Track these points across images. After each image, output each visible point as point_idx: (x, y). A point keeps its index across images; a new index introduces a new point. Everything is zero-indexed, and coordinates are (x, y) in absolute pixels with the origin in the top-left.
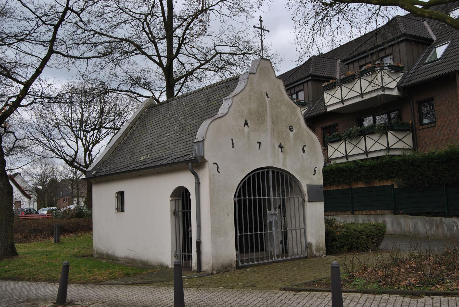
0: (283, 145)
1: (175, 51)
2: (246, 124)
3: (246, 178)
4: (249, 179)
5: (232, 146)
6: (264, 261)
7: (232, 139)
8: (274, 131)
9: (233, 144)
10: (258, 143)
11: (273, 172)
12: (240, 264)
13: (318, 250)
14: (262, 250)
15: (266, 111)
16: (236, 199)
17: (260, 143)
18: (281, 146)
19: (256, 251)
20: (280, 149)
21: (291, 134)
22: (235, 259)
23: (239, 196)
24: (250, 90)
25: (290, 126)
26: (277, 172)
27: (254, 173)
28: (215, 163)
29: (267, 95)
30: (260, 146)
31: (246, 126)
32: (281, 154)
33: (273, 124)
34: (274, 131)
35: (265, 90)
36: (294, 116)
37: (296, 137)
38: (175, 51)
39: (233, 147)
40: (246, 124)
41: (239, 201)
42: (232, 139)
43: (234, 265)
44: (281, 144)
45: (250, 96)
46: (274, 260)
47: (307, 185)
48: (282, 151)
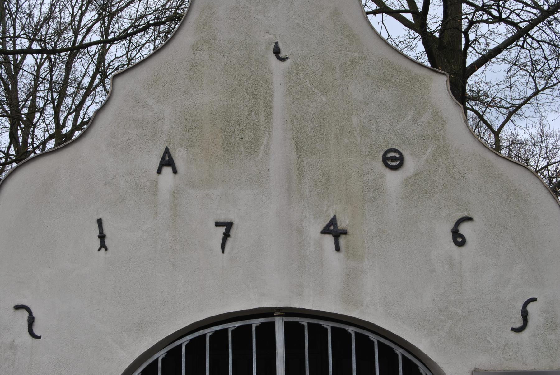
0: (342, 224)
1: (61, 122)
2: (167, 161)
3: (160, 355)
5: (98, 243)
7: (100, 222)
8: (300, 176)
9: (102, 237)
10: (218, 224)
11: (293, 332)
15: (268, 107)
17: (229, 226)
18: (333, 230)
20: (329, 240)
21: (393, 180)
24: (195, 47)
25: (385, 160)
26: (363, 341)
27: (201, 333)
29: (277, 52)
30: (227, 235)
31: (167, 171)
33: (297, 149)
34: (300, 176)
38: (61, 122)
39: (103, 246)
40: (167, 161)
42: (100, 222)
48: (338, 249)
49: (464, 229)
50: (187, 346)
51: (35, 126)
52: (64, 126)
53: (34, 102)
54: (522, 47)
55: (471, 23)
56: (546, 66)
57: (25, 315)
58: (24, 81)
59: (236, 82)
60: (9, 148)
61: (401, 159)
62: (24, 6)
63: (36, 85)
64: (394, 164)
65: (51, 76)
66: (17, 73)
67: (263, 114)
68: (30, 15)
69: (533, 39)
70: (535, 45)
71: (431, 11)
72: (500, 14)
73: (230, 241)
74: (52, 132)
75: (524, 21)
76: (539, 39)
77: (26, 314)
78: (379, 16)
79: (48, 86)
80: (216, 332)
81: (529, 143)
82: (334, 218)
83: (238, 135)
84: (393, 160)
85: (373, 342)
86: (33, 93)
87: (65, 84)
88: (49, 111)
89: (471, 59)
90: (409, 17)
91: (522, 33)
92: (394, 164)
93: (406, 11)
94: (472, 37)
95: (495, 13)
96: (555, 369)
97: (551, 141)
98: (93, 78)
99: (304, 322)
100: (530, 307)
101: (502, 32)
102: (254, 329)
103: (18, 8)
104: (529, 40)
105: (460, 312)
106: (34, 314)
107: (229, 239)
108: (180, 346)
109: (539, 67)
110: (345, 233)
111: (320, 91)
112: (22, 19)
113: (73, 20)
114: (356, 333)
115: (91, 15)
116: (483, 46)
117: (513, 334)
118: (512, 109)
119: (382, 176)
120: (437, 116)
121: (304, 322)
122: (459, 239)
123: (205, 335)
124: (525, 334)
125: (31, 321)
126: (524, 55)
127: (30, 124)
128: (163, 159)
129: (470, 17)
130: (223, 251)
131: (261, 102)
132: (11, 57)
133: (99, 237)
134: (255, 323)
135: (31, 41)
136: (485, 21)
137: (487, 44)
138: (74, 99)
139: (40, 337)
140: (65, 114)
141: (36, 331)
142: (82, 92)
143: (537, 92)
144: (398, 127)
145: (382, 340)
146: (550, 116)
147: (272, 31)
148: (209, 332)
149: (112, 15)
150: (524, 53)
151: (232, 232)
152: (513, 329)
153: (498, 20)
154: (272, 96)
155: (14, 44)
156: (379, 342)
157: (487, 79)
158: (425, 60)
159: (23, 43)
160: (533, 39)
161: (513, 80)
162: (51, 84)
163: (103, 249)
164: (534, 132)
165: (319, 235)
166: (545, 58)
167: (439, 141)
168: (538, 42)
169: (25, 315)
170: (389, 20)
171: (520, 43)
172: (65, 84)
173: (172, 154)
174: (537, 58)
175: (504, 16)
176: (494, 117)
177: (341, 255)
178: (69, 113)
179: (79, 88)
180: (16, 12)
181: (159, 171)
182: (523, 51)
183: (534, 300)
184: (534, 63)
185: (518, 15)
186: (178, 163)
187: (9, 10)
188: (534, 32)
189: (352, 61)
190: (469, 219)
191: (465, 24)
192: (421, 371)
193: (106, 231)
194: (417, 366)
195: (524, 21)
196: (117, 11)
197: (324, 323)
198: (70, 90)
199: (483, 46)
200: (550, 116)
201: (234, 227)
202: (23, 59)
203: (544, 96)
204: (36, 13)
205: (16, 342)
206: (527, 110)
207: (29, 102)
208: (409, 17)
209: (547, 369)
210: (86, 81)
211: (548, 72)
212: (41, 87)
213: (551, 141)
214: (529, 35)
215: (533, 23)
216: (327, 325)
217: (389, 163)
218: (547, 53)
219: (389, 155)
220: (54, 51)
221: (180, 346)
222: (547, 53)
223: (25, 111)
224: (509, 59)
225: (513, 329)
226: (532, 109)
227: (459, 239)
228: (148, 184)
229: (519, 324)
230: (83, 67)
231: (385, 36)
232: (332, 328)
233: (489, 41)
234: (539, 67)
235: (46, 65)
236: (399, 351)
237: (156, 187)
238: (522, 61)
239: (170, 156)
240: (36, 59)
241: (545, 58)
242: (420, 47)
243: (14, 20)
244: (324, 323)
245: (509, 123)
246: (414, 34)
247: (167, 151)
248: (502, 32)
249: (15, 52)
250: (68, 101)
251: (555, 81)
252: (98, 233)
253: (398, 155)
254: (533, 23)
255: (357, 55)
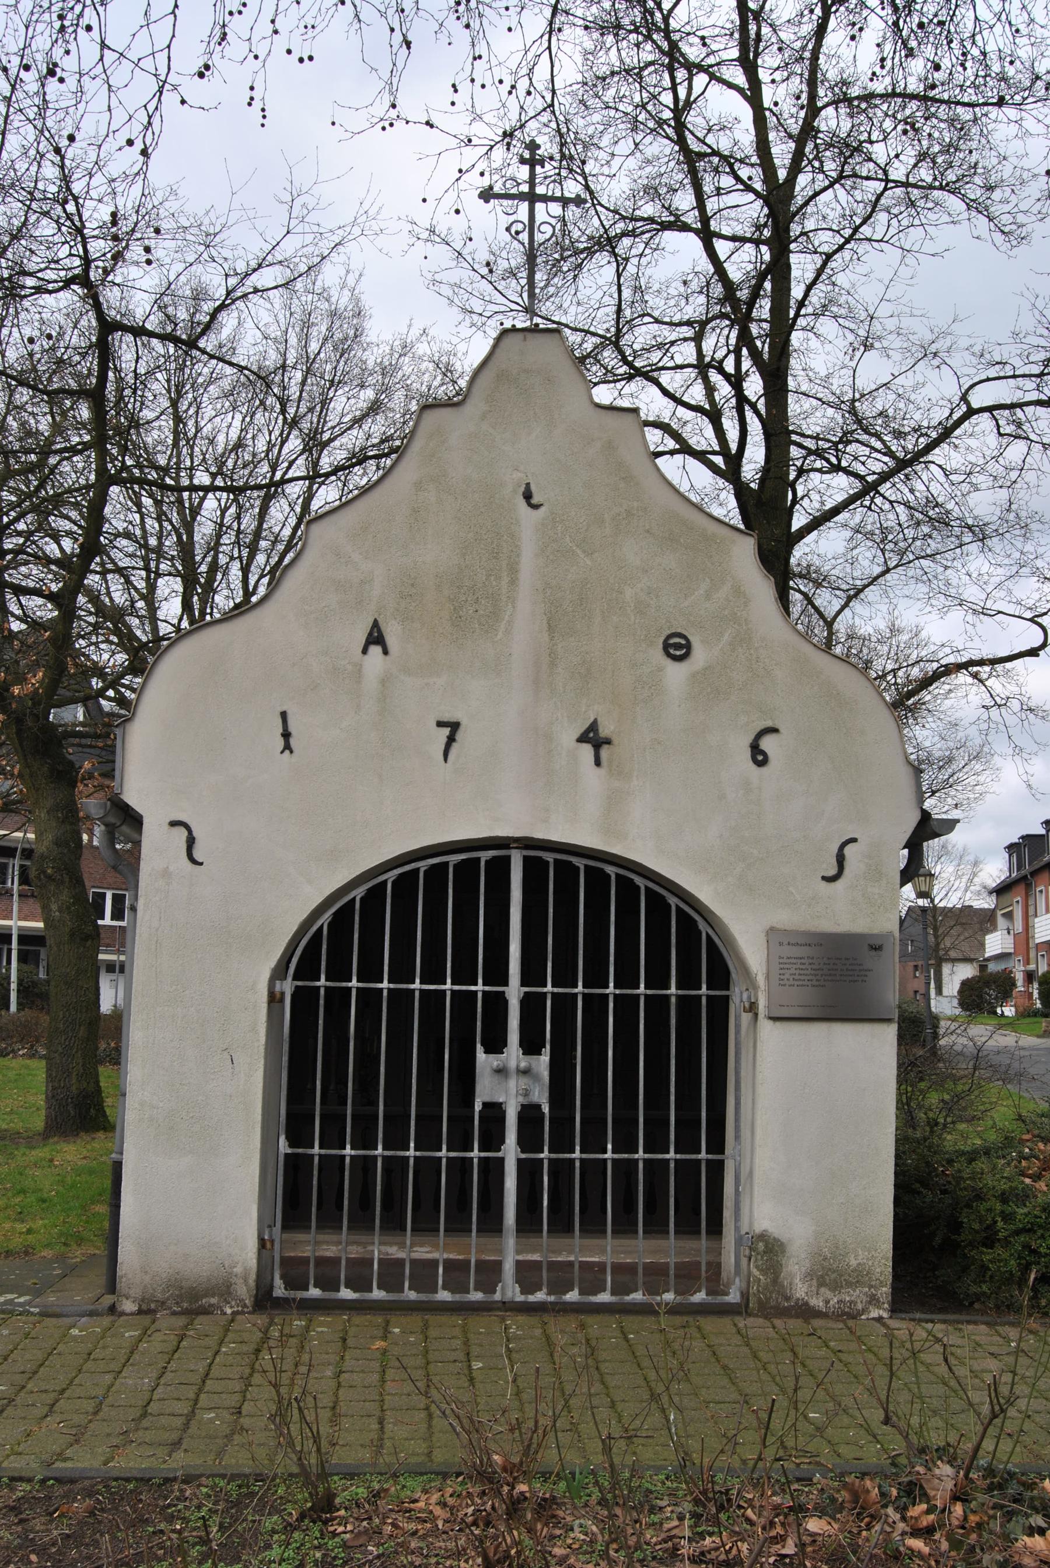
0: (605, 730)
2: (376, 638)
3: (359, 893)
4: (376, 894)
5: (280, 743)
6: (371, 1291)
7: (284, 715)
8: (553, 664)
9: (286, 735)
10: (440, 724)
11: (534, 870)
12: (279, 1290)
13: (828, 1273)
14: (716, 1228)
15: (513, 570)
16: (287, 987)
18: (593, 738)
19: (709, 1232)
20: (587, 750)
21: (676, 673)
22: (252, 1262)
23: (307, 968)
24: (418, 486)
25: (666, 647)
26: (627, 889)
28: (173, 824)
29: (528, 496)
30: (451, 739)
31: (375, 650)
32: (592, 778)
33: (551, 629)
34: (553, 664)
35: (517, 475)
36: (704, 586)
37: (708, 689)
39: (287, 747)
40: (376, 638)
41: (303, 999)
42: (284, 715)
43: (244, 1291)
44: (593, 727)
45: (415, 511)
46: (497, 1296)
47: (771, 931)
48: (598, 763)
49: (767, 744)
50: (393, 883)
51: (215, 592)
52: (254, 593)
53: (215, 558)
54: (869, 508)
55: (801, 472)
56: (901, 536)
57: (182, 834)
58: (204, 530)
59: (471, 535)
60: (180, 620)
61: (688, 646)
62: (205, 430)
63: (219, 536)
64: (678, 653)
65: (239, 524)
66: (194, 519)
67: (505, 580)
68: (212, 442)
69: (884, 497)
70: (887, 506)
71: (747, 454)
72: (839, 461)
73: (455, 748)
74: (238, 601)
75: (874, 473)
76: (893, 498)
77: (184, 833)
78: (679, 458)
79: (233, 539)
80: (433, 866)
81: (874, 639)
82: (595, 722)
83: (470, 605)
84: (677, 648)
85: (638, 887)
86: (214, 547)
87: (257, 534)
88: (235, 570)
89: (798, 521)
90: (718, 460)
91: (869, 489)
92: (678, 653)
93: (714, 453)
94: (800, 490)
95: (834, 460)
96: (875, 932)
97: (904, 637)
98: (295, 529)
99: (549, 857)
100: (848, 850)
101: (841, 486)
102: (483, 864)
103: (197, 432)
104: (878, 500)
105: (755, 852)
106: (195, 834)
107: (454, 744)
108: (386, 881)
109: (890, 537)
110: (608, 742)
111: (584, 552)
112: (200, 445)
113: (268, 452)
114: (617, 875)
115: (294, 443)
116: (817, 505)
117: (824, 883)
118: (852, 593)
119: (660, 669)
120: (738, 591)
121: (549, 857)
122: (759, 757)
123: (418, 869)
124: (839, 884)
125: (191, 841)
126: (870, 520)
127: (210, 589)
128: (370, 634)
129: (799, 463)
130: (446, 760)
131: (504, 563)
132: (186, 495)
133: (283, 735)
134: (485, 856)
135: (214, 476)
136: (819, 470)
137: (823, 503)
138: (269, 557)
139: (201, 864)
140: (256, 577)
141: (197, 855)
142: (281, 547)
143: (888, 571)
144: (686, 604)
145: (651, 885)
146: (902, 604)
147: (522, 468)
148: (423, 865)
149: (325, 444)
150: (872, 517)
151: (459, 736)
152: (824, 878)
153: (837, 468)
154: (518, 556)
155: (191, 477)
156: (647, 888)
157: (819, 549)
158: (737, 521)
159: (202, 478)
160: (884, 497)
161: (855, 552)
162: (237, 536)
163: (287, 752)
164: (882, 625)
165: (573, 743)
166: (900, 525)
167: (740, 625)
168: (891, 502)
169: (182, 834)
170: (693, 463)
171: (867, 503)
172: (257, 534)
173: (383, 629)
174: (889, 524)
175: (844, 464)
176: (828, 601)
177: (602, 772)
178: (262, 576)
179: (274, 543)
180: (195, 436)
181: (365, 651)
182: (870, 513)
183: (854, 840)
184: (884, 531)
185: (863, 463)
186: (391, 640)
187: (185, 434)
188: (885, 488)
189: (629, 513)
190: (774, 730)
191: (792, 476)
192: (701, 927)
193: (292, 728)
194: (695, 922)
195: (874, 473)
196: (331, 440)
197: (575, 860)
198: (263, 544)
199: (817, 505)
200: (902, 604)
201: (462, 729)
202: (203, 500)
203: (896, 576)
204: (221, 439)
205: (171, 868)
206: (871, 593)
207: (209, 559)
208: (718, 460)
209: (866, 931)
210: (287, 532)
211: (902, 544)
212: (225, 540)
213: (904, 637)
214: (878, 492)
215: (885, 477)
216: (580, 863)
217: (672, 651)
218: (903, 518)
219: (672, 641)
220: (242, 490)
221: (386, 881)
222: (903, 518)
223: (203, 568)
224: (852, 524)
225: (824, 878)
226: (877, 593)
227: (759, 757)
228: (350, 667)
229: (832, 871)
230: (281, 516)
231: (684, 487)
232: (586, 866)
233: (825, 498)
234: (890, 537)
235: (232, 510)
236: (673, 901)
237: (360, 671)
238: (869, 527)
239: (379, 631)
240: (219, 500)
241: (900, 525)
242: (733, 502)
243: (192, 448)
244: (575, 860)
245: (847, 611)
246: (721, 482)
247: (376, 624)
248: (841, 486)
249: (193, 488)
250: (261, 558)
251: (911, 557)
252: (281, 731)
253: (683, 642)
254: (885, 477)
255: (635, 504)
